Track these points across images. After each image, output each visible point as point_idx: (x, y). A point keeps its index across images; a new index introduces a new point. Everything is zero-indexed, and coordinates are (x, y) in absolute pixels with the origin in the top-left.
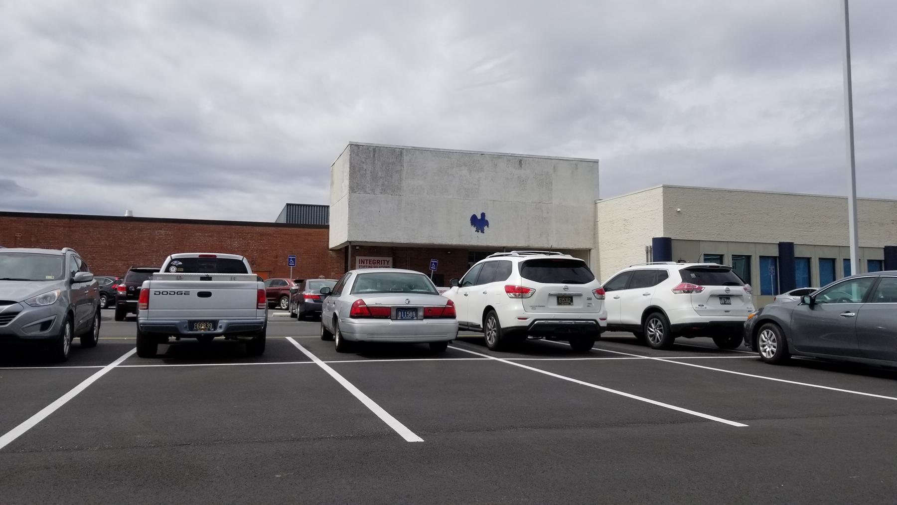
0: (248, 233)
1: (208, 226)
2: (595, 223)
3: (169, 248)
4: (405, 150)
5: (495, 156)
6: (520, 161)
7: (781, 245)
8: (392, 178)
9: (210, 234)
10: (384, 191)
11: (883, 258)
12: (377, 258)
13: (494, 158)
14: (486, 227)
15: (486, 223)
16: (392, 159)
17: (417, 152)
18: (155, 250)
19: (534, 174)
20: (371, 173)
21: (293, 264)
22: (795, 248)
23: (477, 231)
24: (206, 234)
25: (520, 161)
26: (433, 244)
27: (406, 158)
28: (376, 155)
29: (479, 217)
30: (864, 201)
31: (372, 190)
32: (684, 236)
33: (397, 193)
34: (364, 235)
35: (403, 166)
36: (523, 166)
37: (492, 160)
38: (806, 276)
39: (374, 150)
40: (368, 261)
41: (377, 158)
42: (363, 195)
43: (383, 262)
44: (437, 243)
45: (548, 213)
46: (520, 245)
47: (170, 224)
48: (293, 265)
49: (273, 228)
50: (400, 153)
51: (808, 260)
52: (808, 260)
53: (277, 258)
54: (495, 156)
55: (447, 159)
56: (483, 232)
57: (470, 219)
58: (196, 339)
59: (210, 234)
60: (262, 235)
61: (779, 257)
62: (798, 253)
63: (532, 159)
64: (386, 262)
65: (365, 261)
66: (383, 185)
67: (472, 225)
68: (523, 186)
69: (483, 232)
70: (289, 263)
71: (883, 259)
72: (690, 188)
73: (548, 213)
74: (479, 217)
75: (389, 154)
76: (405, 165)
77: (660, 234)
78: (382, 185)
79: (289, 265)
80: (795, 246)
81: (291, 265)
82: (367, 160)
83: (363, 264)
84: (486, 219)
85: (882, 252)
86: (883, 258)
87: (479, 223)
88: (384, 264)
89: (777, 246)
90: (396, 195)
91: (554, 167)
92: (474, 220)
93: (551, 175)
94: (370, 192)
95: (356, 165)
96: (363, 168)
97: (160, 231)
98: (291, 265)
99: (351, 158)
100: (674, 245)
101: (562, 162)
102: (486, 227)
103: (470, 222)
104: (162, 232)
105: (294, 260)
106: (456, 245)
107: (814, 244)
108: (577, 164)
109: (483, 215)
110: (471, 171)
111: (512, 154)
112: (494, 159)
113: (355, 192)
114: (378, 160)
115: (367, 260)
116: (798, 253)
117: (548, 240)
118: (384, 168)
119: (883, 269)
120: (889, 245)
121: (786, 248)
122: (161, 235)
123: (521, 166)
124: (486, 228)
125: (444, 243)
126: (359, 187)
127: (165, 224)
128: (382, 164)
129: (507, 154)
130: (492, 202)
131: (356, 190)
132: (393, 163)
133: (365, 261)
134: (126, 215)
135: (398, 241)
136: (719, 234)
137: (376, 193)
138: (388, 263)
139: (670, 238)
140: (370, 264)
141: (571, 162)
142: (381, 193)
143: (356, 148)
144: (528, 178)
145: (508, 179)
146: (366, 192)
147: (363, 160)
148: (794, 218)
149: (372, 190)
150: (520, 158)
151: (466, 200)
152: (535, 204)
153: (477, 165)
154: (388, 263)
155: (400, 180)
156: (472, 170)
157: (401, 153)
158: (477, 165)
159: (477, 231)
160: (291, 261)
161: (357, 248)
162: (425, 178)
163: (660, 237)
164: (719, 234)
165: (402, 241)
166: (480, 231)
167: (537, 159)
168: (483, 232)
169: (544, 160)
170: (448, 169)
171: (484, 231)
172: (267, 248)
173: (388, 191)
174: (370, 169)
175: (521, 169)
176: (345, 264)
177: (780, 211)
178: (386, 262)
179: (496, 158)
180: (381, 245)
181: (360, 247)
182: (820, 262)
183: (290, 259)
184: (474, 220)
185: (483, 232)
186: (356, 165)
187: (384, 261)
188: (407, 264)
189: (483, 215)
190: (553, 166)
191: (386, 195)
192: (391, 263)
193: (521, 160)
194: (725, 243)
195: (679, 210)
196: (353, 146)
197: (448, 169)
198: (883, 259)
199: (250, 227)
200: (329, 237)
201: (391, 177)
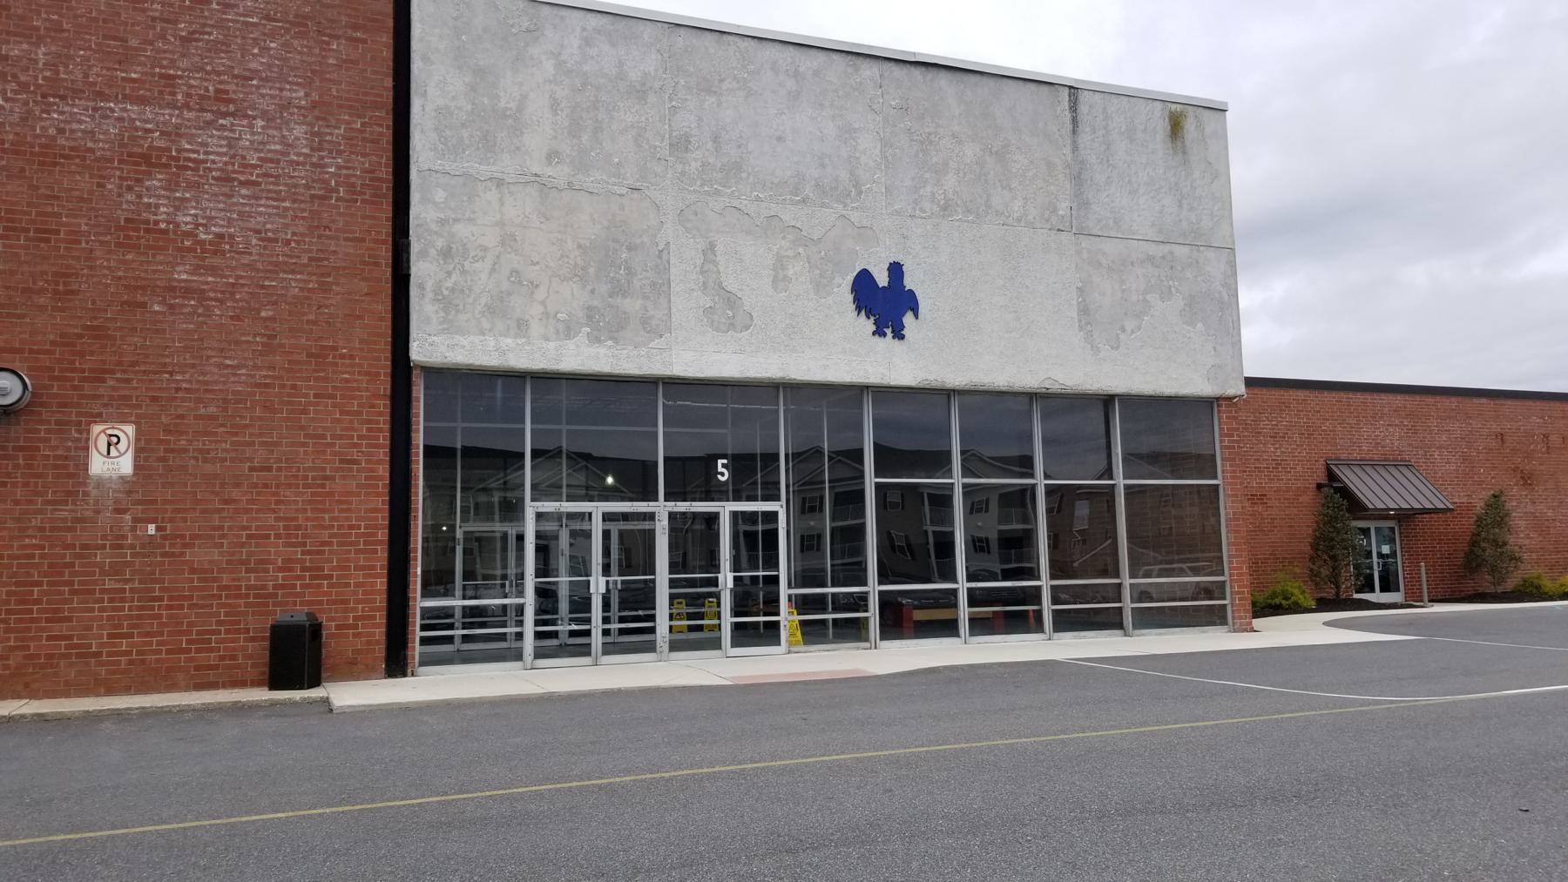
6: (1176, 125)
15: (910, 302)
23: (879, 332)
25: (1176, 125)
29: (882, 279)
56: (899, 335)
67: (859, 309)
69: (902, 337)
74: (882, 279)
80: (266, 677)
92: (863, 285)
103: (850, 297)
109: (896, 270)
119: (588, 615)
124: (908, 319)
159: (879, 332)
166: (889, 331)
168: (899, 335)
171: (877, 336)
180: (441, 366)
184: (863, 285)
185: (902, 337)
189: (896, 270)
192: (452, 585)
200: (724, 23)
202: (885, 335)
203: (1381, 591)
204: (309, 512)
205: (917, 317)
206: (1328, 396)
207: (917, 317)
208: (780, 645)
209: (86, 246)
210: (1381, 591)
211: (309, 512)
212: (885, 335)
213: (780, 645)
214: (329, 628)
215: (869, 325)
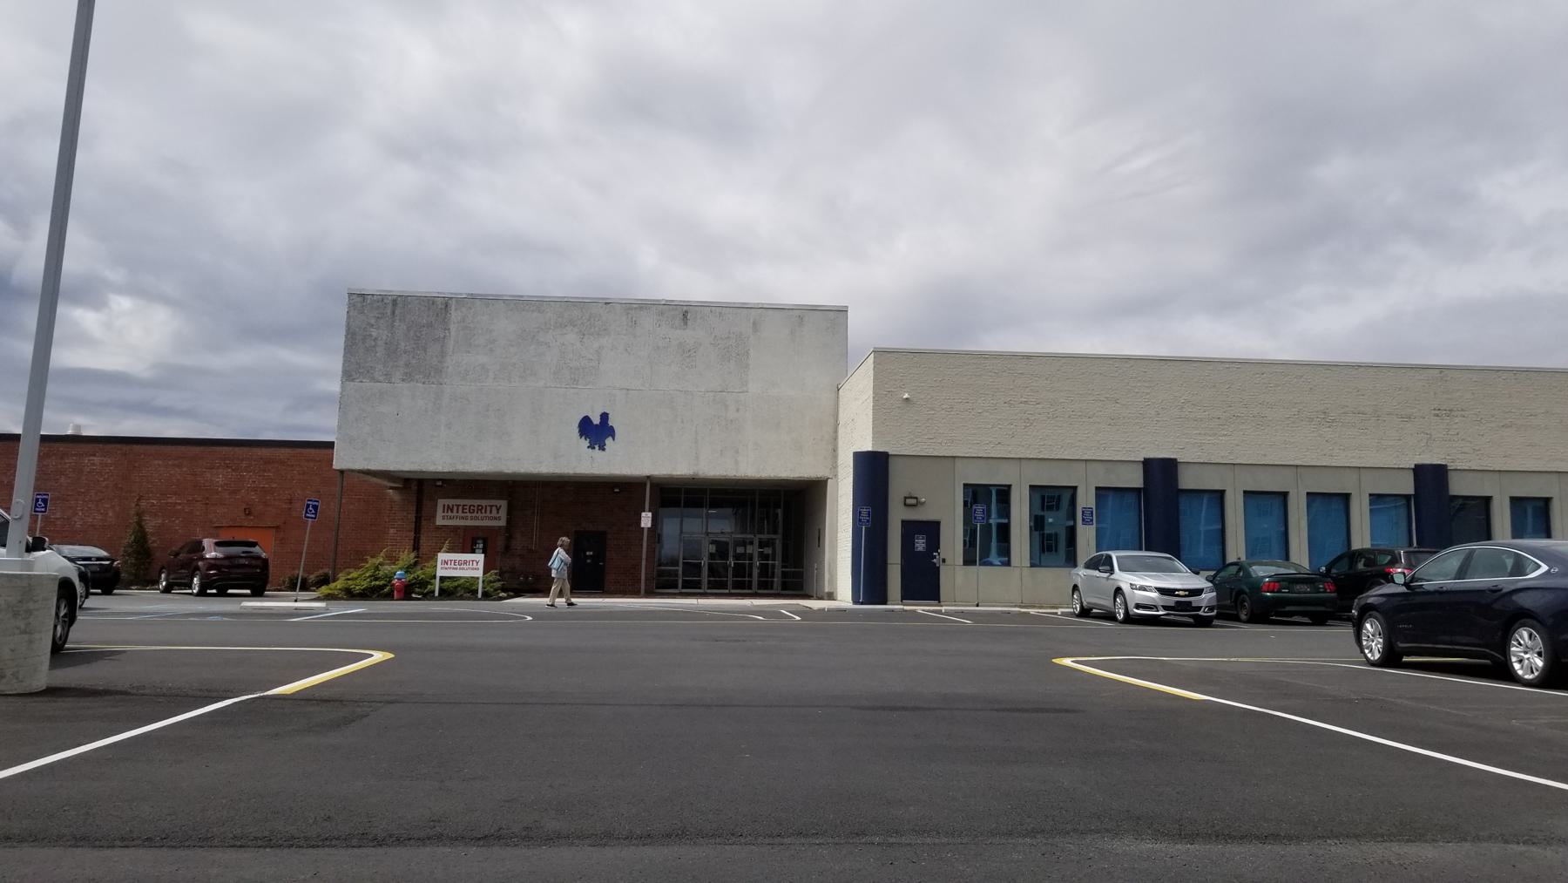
0: (242, 460)
1: (173, 448)
2: (836, 425)
3: (107, 487)
4: (454, 300)
5: (635, 306)
6: (685, 315)
7: (1419, 470)
8: (425, 351)
9: (176, 462)
10: (408, 377)
11: (1410, 490)
12: (476, 502)
13: (632, 309)
14: (610, 438)
15: (611, 432)
16: (428, 316)
17: (478, 302)
18: (83, 490)
19: (713, 337)
20: (386, 343)
21: (313, 516)
22: (1450, 477)
23: (591, 447)
24: (170, 463)
26: (501, 472)
27: (455, 315)
28: (397, 312)
29: (596, 420)
30: (1361, 370)
31: (386, 375)
32: (918, 449)
33: (434, 380)
34: (365, 459)
35: (449, 329)
36: (689, 323)
37: (628, 314)
38: (1283, 529)
39: (395, 302)
40: (460, 508)
41: (398, 318)
42: (367, 384)
43: (488, 508)
44: (510, 471)
45: (738, 410)
46: (679, 473)
47: (109, 447)
48: (312, 518)
49: (288, 450)
50: (443, 307)
51: (1220, 495)
52: (1220, 495)
53: (291, 503)
54: (635, 306)
55: (535, 314)
56: (602, 448)
57: (577, 425)
58: (1488, 662)
59: (176, 462)
60: (268, 462)
61: (1416, 495)
62: (1187, 481)
63: (709, 309)
64: (494, 508)
65: (455, 508)
66: (407, 365)
67: (581, 436)
68: (688, 360)
69: (604, 450)
70: (306, 512)
71: (1413, 493)
72: (1221, 362)
73: (738, 410)
74: (596, 420)
75: (423, 308)
76: (453, 328)
77: (868, 446)
78: (406, 365)
79: (306, 517)
81: (308, 517)
82: (382, 321)
83: (450, 514)
84: (610, 424)
85: (1410, 477)
86: (1410, 490)
87: (596, 431)
88: (491, 512)
89: (1141, 467)
90: (433, 383)
91: (754, 323)
93: (748, 338)
94: (381, 378)
95: (357, 330)
96: (371, 335)
97: (92, 458)
98: (308, 517)
99: (348, 318)
100: (895, 468)
101: (770, 312)
102: (610, 438)
104: (96, 460)
105: (315, 507)
106: (548, 473)
107: (1018, 456)
108: (801, 315)
109: (605, 417)
110: (584, 335)
111: (667, 301)
112: (630, 312)
113: (353, 380)
114: (400, 320)
115: (458, 506)
116: (1187, 481)
117: (737, 462)
118: (412, 333)
120: (1152, 456)
121: (1161, 472)
122: (93, 464)
123: (686, 324)
124: (609, 441)
125: (522, 471)
126: (361, 371)
127: (101, 445)
128: (408, 328)
129: (658, 300)
130: (624, 391)
131: (355, 377)
132: (430, 325)
133: (455, 508)
134: (69, 432)
135: (432, 468)
136: (999, 443)
137: (393, 380)
138: (498, 510)
139: (1176, 459)
140: (463, 512)
141: (791, 312)
142: (403, 380)
143: (359, 299)
144: (700, 345)
145: (658, 347)
146: (374, 380)
147: (373, 321)
148: (1182, 408)
149: (386, 375)
150: (685, 308)
151: (572, 391)
152: (712, 394)
153: (596, 323)
154: (498, 510)
155: (443, 354)
156: (585, 333)
157: (447, 306)
158: (596, 323)
159: (591, 447)
160: (40, 503)
161: (440, 483)
162: (491, 350)
163: (865, 450)
164: (999, 443)
165: (440, 469)
166: (597, 447)
167: (718, 310)
168: (602, 448)
169: (735, 310)
170: (538, 332)
171: (590, 449)
172: (274, 486)
173: (417, 377)
174: (384, 338)
175: (684, 329)
176: (417, 513)
177: (1148, 394)
178: (494, 508)
179: (636, 308)
181: (443, 481)
182: (1371, 503)
183: (308, 506)
184: (586, 427)
185: (604, 450)
186: (357, 330)
187: (491, 506)
188: (534, 513)
189: (605, 417)
190: (751, 321)
191: (412, 383)
193: (686, 312)
194: (1406, 471)
195: (906, 396)
196: (354, 297)
197: (538, 332)
198: (1413, 493)
199: (245, 449)
201: (425, 350)
202: (594, 448)
203: (1486, 501)
204: (1104, 525)
205: (614, 439)
206: (137, 448)
207: (614, 439)
208: (903, 522)
209: (1109, 553)
210: (1486, 501)
211: (1104, 525)
212: (594, 448)
213: (903, 522)
214: (1494, 498)
215: (587, 443)
